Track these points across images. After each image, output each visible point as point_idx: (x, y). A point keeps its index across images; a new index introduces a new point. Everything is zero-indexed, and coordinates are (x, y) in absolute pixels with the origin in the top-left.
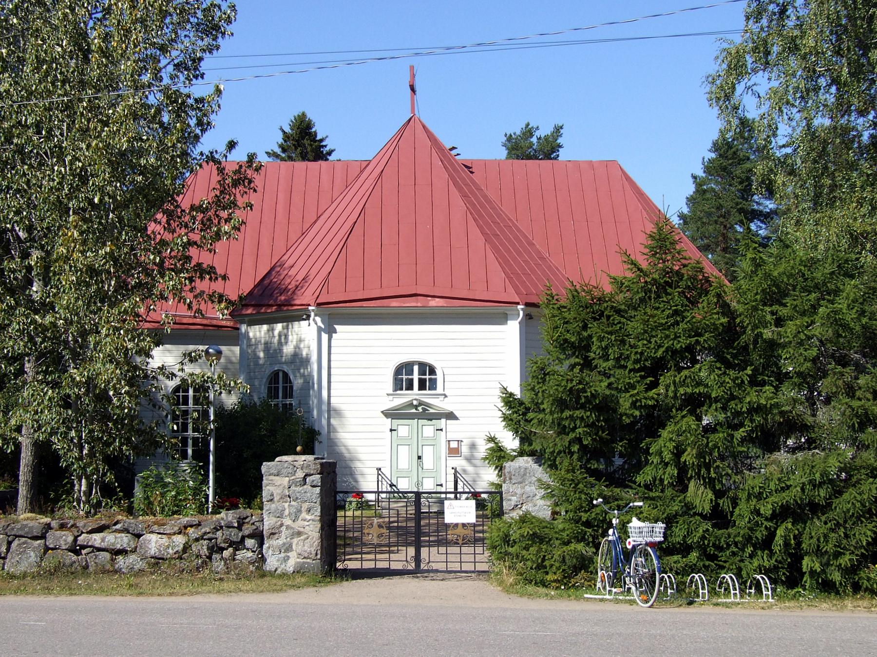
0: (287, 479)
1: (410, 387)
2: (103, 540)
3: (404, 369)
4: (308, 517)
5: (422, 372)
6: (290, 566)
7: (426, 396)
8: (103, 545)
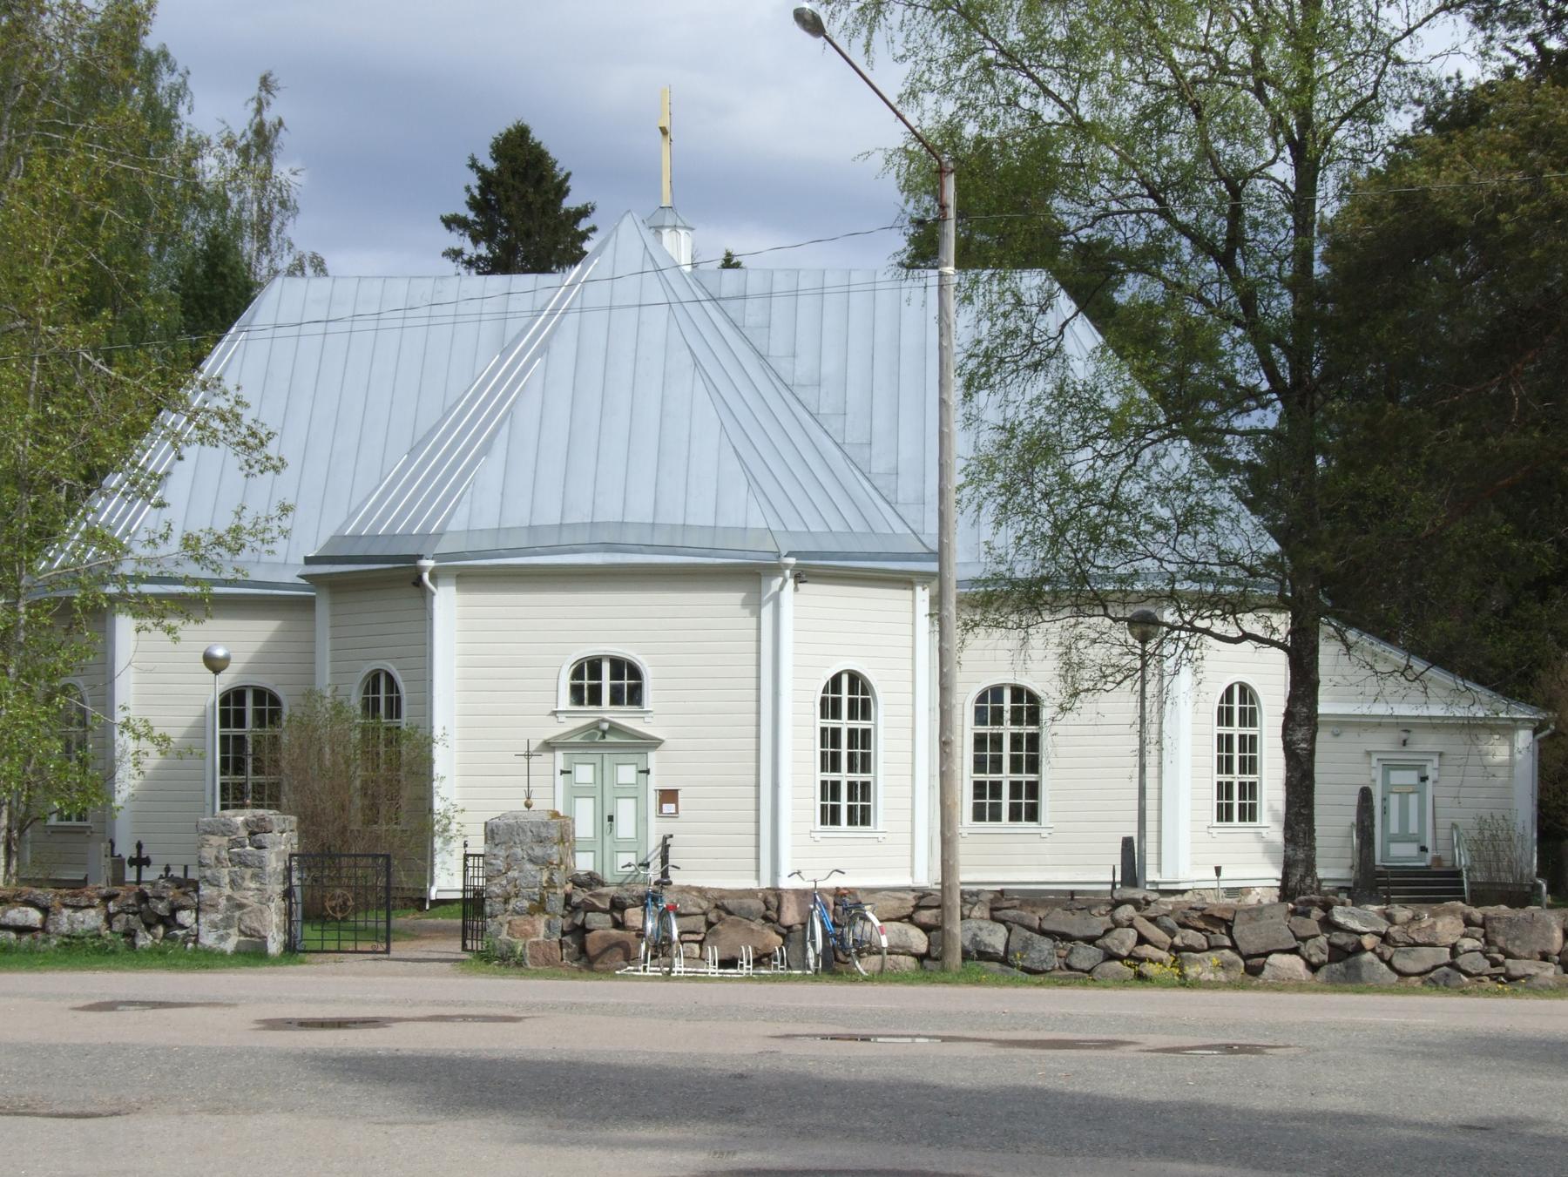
1: (595, 698)
6: (229, 946)
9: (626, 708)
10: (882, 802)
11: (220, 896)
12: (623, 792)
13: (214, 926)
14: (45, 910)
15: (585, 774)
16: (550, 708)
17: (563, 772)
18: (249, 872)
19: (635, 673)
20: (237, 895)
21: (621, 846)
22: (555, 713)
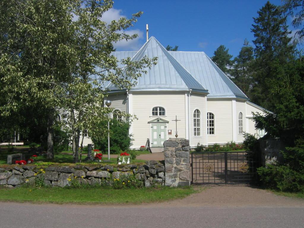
0: (174, 148)
1: (157, 114)
2: (97, 173)
3: (155, 109)
4: (184, 164)
5: (160, 110)
6: (176, 184)
7: (162, 117)
8: (97, 176)
9: (162, 116)
10: (201, 131)
11: (173, 167)
12: (162, 130)
13: (171, 177)
14: (111, 172)
15: (155, 127)
16: (148, 116)
17: (151, 127)
18: (183, 159)
19: (163, 109)
20: (178, 167)
21: (161, 140)
22: (150, 117)
